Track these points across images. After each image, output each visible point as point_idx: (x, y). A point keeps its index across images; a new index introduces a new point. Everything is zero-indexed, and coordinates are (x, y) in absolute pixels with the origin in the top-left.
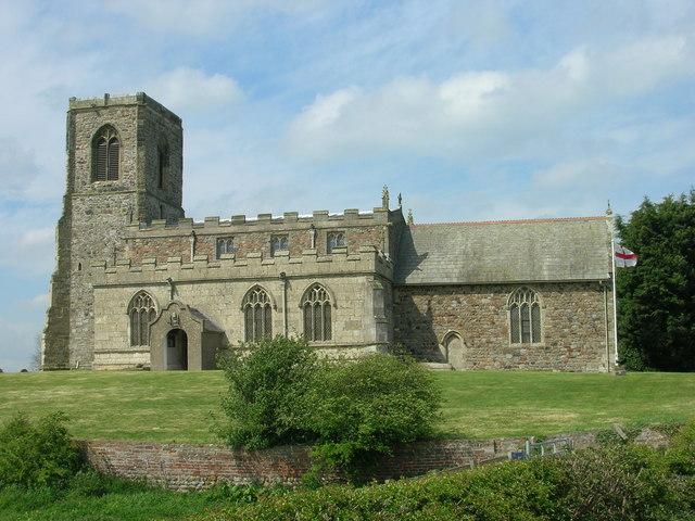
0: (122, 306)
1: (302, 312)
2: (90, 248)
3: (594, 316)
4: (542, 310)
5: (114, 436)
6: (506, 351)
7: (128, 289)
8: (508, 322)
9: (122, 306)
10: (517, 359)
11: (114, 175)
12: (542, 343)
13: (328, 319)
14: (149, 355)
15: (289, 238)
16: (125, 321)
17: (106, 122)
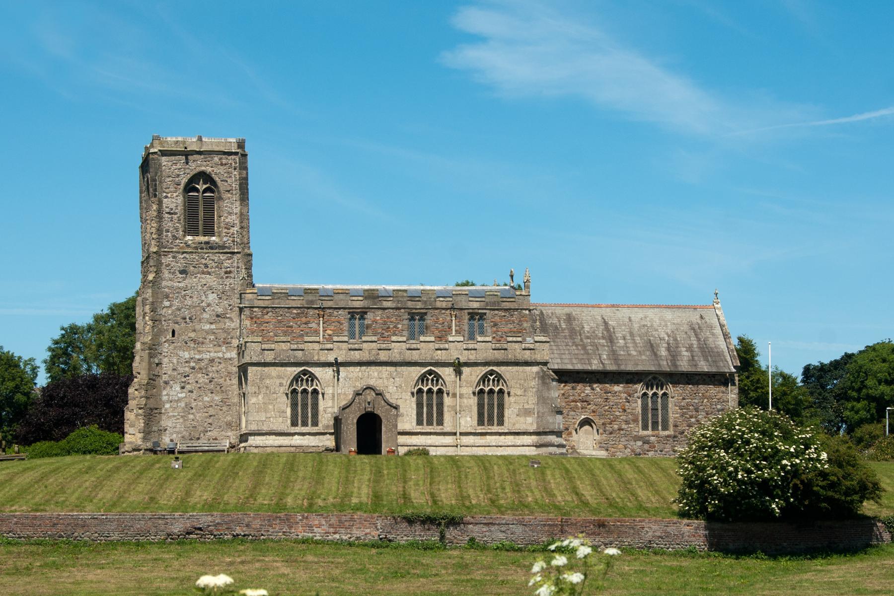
0: (281, 385)
1: (476, 398)
2: (187, 314)
3: (719, 407)
4: (670, 399)
5: (153, 465)
6: (637, 438)
7: (289, 369)
8: (639, 409)
9: (281, 385)
10: (646, 447)
11: (209, 230)
12: (670, 432)
13: (501, 406)
14: (333, 437)
15: (428, 317)
16: (285, 405)
17: (203, 168)
